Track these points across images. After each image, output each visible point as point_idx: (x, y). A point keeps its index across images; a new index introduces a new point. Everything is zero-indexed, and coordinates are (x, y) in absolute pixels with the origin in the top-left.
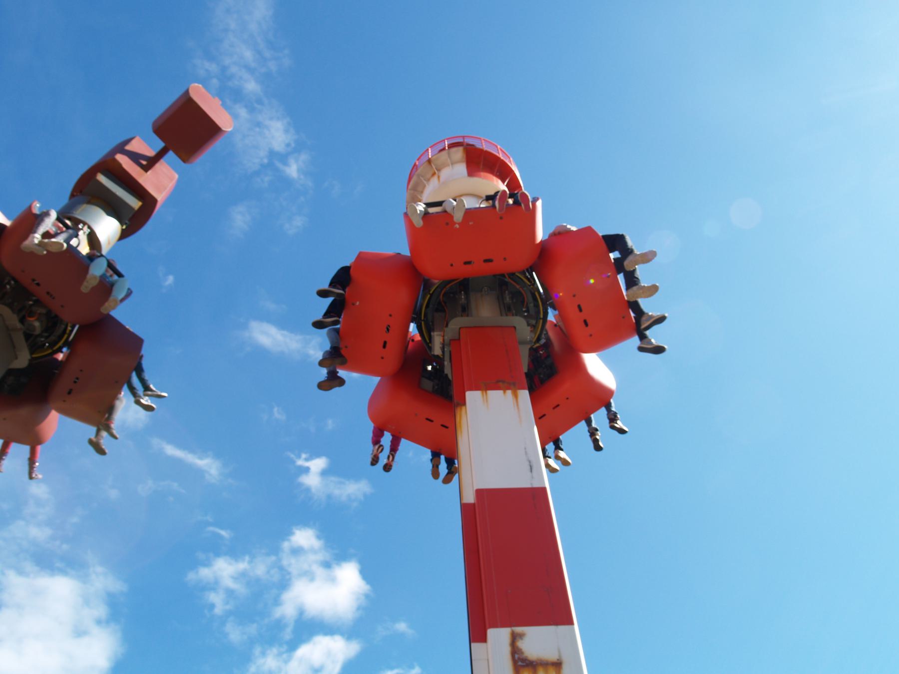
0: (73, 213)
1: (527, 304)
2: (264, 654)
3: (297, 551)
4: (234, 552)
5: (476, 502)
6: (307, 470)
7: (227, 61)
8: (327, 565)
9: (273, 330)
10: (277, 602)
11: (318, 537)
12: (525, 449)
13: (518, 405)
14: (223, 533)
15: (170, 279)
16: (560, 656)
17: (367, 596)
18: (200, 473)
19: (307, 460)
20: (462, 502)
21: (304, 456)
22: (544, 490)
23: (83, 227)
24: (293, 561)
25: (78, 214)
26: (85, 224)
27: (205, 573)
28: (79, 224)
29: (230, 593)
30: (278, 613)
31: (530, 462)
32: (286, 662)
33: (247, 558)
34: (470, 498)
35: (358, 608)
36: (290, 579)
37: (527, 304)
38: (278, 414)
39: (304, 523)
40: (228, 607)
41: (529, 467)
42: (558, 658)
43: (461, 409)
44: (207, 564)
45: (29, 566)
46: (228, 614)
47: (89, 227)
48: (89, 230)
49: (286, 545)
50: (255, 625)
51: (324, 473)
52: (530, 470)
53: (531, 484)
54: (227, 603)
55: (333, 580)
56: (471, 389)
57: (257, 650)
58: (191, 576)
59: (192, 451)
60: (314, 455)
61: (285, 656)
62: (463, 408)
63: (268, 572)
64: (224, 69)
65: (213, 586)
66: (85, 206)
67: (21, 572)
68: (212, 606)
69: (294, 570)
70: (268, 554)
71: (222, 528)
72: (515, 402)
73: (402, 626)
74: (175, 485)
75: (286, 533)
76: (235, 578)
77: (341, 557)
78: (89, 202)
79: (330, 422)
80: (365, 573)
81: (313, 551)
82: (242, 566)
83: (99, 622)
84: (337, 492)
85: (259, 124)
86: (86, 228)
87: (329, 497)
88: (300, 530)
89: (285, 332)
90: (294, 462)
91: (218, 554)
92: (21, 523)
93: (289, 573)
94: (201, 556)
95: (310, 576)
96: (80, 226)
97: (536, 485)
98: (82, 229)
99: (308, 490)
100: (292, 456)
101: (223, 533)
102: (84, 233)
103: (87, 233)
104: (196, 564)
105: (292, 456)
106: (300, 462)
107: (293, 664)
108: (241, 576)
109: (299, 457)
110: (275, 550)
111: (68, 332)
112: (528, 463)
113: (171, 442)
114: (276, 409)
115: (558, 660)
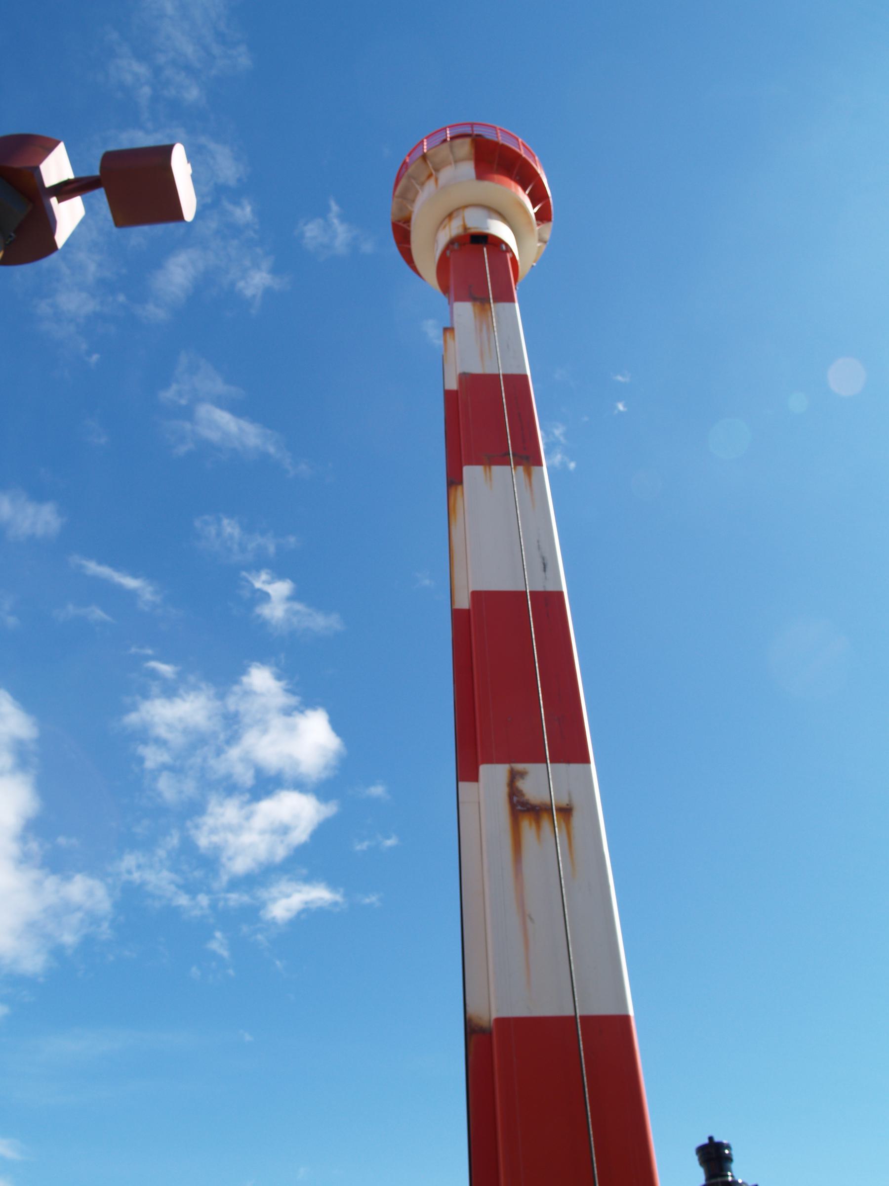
7: (161, 59)
11: (278, 678)
12: (538, 542)
16: (570, 800)
18: (132, 595)
20: (453, 608)
22: (560, 594)
27: (133, 718)
31: (543, 558)
35: (326, 767)
38: (230, 528)
41: (542, 566)
42: (567, 802)
43: (456, 490)
44: (134, 708)
52: (543, 569)
55: (292, 729)
56: (470, 463)
62: (459, 488)
73: (377, 790)
80: (336, 725)
97: (550, 588)
106: (258, 585)
114: (226, 522)
115: (568, 805)
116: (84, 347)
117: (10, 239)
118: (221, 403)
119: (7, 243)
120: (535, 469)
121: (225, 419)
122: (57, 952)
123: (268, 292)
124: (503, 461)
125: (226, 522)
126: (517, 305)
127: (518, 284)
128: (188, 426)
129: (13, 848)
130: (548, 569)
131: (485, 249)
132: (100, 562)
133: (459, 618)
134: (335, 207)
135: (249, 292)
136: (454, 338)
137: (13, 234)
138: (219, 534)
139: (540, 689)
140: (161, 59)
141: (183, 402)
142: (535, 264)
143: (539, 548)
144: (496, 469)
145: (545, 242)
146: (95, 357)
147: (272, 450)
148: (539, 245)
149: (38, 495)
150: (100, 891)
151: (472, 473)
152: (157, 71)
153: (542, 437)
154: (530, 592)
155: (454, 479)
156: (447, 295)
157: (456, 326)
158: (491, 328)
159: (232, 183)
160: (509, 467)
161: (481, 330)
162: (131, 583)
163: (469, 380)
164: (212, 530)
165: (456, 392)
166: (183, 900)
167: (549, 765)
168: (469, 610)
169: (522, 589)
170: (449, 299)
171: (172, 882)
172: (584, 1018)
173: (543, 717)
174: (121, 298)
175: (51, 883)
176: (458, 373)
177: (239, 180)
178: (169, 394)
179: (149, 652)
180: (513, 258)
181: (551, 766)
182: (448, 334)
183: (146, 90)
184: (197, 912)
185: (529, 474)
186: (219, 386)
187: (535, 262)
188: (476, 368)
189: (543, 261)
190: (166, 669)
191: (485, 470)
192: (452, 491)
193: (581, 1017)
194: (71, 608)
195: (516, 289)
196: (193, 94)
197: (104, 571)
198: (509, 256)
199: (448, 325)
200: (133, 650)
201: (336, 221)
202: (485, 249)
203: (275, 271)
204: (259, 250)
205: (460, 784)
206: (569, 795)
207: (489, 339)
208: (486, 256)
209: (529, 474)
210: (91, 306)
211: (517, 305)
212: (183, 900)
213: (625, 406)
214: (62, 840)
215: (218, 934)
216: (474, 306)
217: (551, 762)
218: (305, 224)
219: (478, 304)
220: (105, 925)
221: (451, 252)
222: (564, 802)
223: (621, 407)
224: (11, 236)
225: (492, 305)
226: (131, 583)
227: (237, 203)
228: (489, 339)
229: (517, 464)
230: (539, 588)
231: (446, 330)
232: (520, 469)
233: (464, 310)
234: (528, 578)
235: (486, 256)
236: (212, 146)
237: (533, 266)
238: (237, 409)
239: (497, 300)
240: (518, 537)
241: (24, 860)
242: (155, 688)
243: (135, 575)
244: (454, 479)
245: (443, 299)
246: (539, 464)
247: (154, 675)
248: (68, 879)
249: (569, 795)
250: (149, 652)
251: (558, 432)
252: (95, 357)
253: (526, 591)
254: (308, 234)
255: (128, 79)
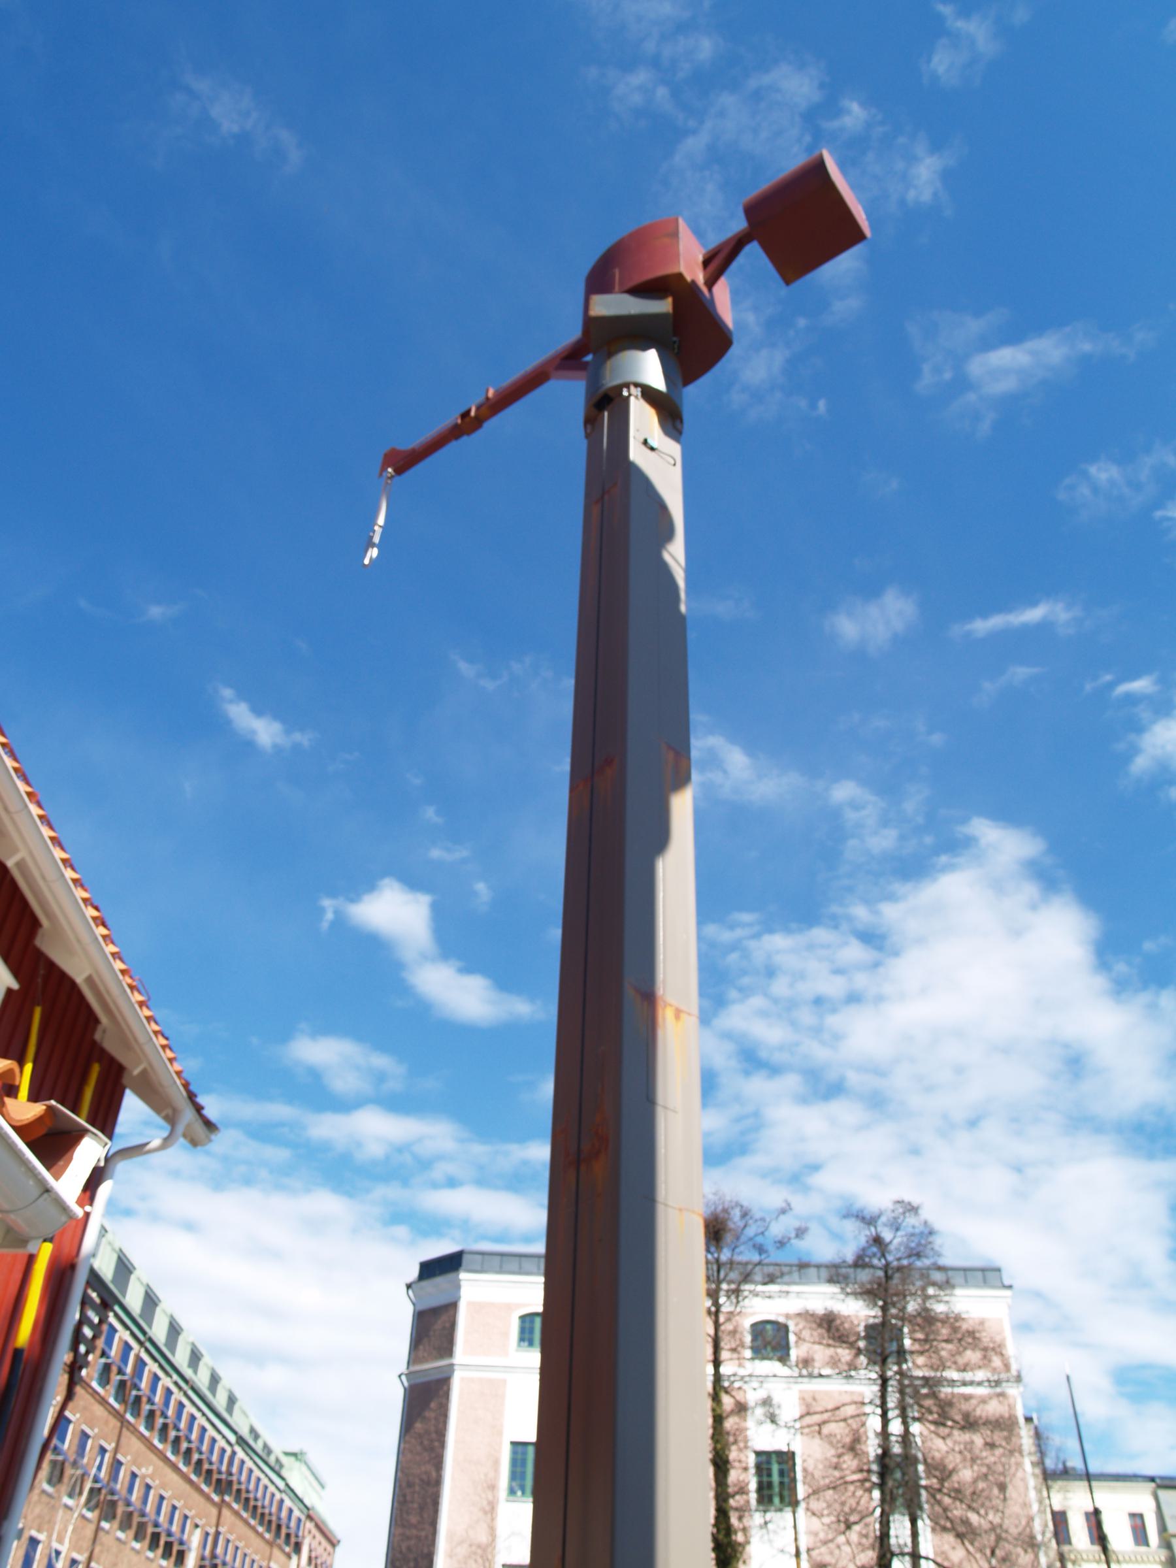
0: (603, 385)
1: (69, 1483)
7: (650, 47)
18: (1044, 626)
23: (629, 391)
25: (610, 381)
26: (627, 385)
27: (1140, 764)
28: (622, 391)
37: (69, 1483)
38: (1103, 473)
44: (1135, 750)
45: (898, 887)
47: (636, 385)
48: (639, 389)
64: (655, 62)
66: (609, 364)
67: (891, 898)
78: (610, 354)
83: (1034, 907)
85: (757, 95)
86: (632, 388)
92: (852, 843)
96: (625, 393)
98: (630, 395)
102: (636, 397)
103: (639, 394)
111: (968, 1376)
114: (1093, 470)
116: (803, 404)
117: (676, 346)
118: (987, 344)
119: (676, 351)
121: (1006, 357)
123: (947, 176)
125: (1093, 470)
128: (972, 397)
129: (1100, 982)
131: (606, 414)
132: (985, 615)
134: (946, 10)
135: (926, 196)
137: (675, 339)
138: (1095, 489)
140: (650, 47)
141: (948, 375)
146: (822, 405)
147: (1087, 347)
149: (871, 590)
152: (655, 62)
159: (817, 97)
162: (1034, 615)
164: (1085, 490)
174: (802, 322)
177: (822, 86)
178: (926, 381)
179: (1108, 678)
183: (662, 92)
186: (974, 326)
190: (1141, 685)
193: (504, 1381)
194: (987, 685)
196: (706, 47)
197: (996, 622)
200: (1088, 687)
201: (960, 24)
202: (606, 414)
203: (936, 147)
204: (901, 140)
210: (779, 357)
214: (1148, 946)
218: (929, 61)
224: (675, 342)
226: (1034, 615)
227: (839, 112)
236: (766, 79)
238: (1012, 335)
241: (1120, 988)
242: (1145, 714)
243: (1034, 604)
247: (1131, 700)
250: (1108, 678)
252: (822, 405)
254: (941, 70)
255: (637, 99)
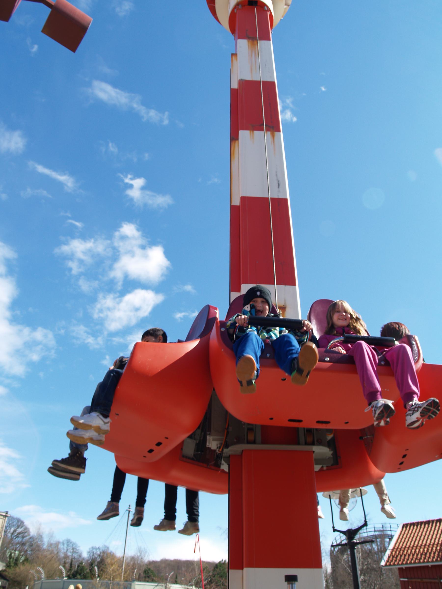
2: (105, 298)
3: (124, 238)
4: (84, 237)
5: (240, 205)
6: (131, 186)
8: (143, 247)
9: (108, 88)
10: (111, 268)
11: (138, 230)
12: (276, 172)
13: (274, 142)
14: (78, 224)
15: (35, 48)
16: (285, 303)
17: (167, 268)
18: (61, 185)
19: (131, 179)
20: (231, 205)
21: (129, 176)
22: (286, 200)
24: (121, 244)
27: (65, 249)
29: (81, 262)
30: (112, 274)
31: (278, 181)
32: (118, 303)
33: (93, 240)
34: (237, 202)
35: (162, 275)
36: (119, 255)
38: (112, 148)
39: (130, 220)
40: (80, 270)
41: (278, 185)
42: (284, 304)
43: (235, 143)
44: (66, 243)
46: (81, 274)
49: (117, 234)
50: (97, 282)
51: (143, 188)
52: (278, 186)
53: (278, 196)
54: (80, 268)
55: (146, 257)
56: (243, 129)
57: (101, 295)
58: (57, 251)
59: (55, 170)
60: (137, 176)
61: (117, 300)
62: (237, 142)
63: (105, 250)
65: (71, 257)
68: (70, 269)
69: (122, 250)
70: (106, 239)
71: (77, 221)
72: (272, 140)
73: (189, 288)
74: (45, 193)
75: (118, 226)
76: (84, 253)
77: (153, 243)
79: (147, 155)
80: (167, 254)
81: (134, 238)
82: (89, 245)
84: (150, 202)
87: (145, 205)
88: (126, 224)
89: (117, 90)
90: (123, 181)
91: (73, 238)
93: (119, 251)
94: (62, 238)
95: (132, 254)
97: (281, 196)
99: (132, 199)
100: (122, 176)
101: (78, 224)
104: (60, 243)
105: (122, 176)
106: (127, 181)
107: (123, 305)
108: (88, 252)
109: (126, 177)
110: (110, 237)
112: (277, 182)
113: (40, 163)
114: (110, 144)
115: (284, 305)
120: (276, 133)
122: (31, 364)
124: (260, 129)
126: (271, 42)
127: (272, 30)
129: (8, 314)
130: (280, 187)
133: (234, 210)
136: (237, 60)
139: (262, 98)
142: (282, 18)
143: (276, 175)
144: (256, 133)
145: (289, 6)
148: (285, 7)
150: (51, 335)
151: (243, 134)
153: (279, 103)
154: (271, 198)
155: (234, 137)
156: (234, 34)
157: (238, 53)
158: (257, 56)
160: (263, 132)
161: (252, 55)
162: (63, 178)
163: (244, 84)
165: (237, 89)
166: (90, 340)
167: (265, 132)
168: (239, 206)
169: (267, 196)
170: (235, 37)
171: (86, 332)
172: (263, 82)
173: (270, 204)
175: (26, 330)
176: (238, 79)
180: (271, 15)
181: (276, 286)
182: (234, 57)
184: (97, 347)
185: (273, 136)
187: (282, 17)
188: (248, 77)
189: (287, 16)
191: (251, 133)
192: (233, 143)
194: (29, 190)
195: (271, 33)
197: (46, 171)
198: (268, 13)
199: (234, 52)
205: (231, 293)
206: (285, 300)
207: (255, 61)
208: (256, 12)
209: (273, 136)
211: (271, 42)
212: (90, 340)
213: (325, 88)
215: (107, 357)
216: (248, 42)
217: (277, 284)
219: (251, 40)
220: (53, 352)
221: (237, 10)
222: (282, 304)
223: (323, 89)
225: (258, 41)
226: (63, 178)
228: (255, 61)
229: (267, 130)
230: (276, 196)
231: (232, 55)
232: (269, 133)
233: (243, 44)
234: (269, 171)
235: (256, 12)
237: (281, 19)
239: (261, 39)
240: (266, 167)
244: (234, 137)
245: (232, 37)
246: (279, 131)
248: (34, 329)
249: (285, 300)
251: (288, 101)
253: (269, 198)
